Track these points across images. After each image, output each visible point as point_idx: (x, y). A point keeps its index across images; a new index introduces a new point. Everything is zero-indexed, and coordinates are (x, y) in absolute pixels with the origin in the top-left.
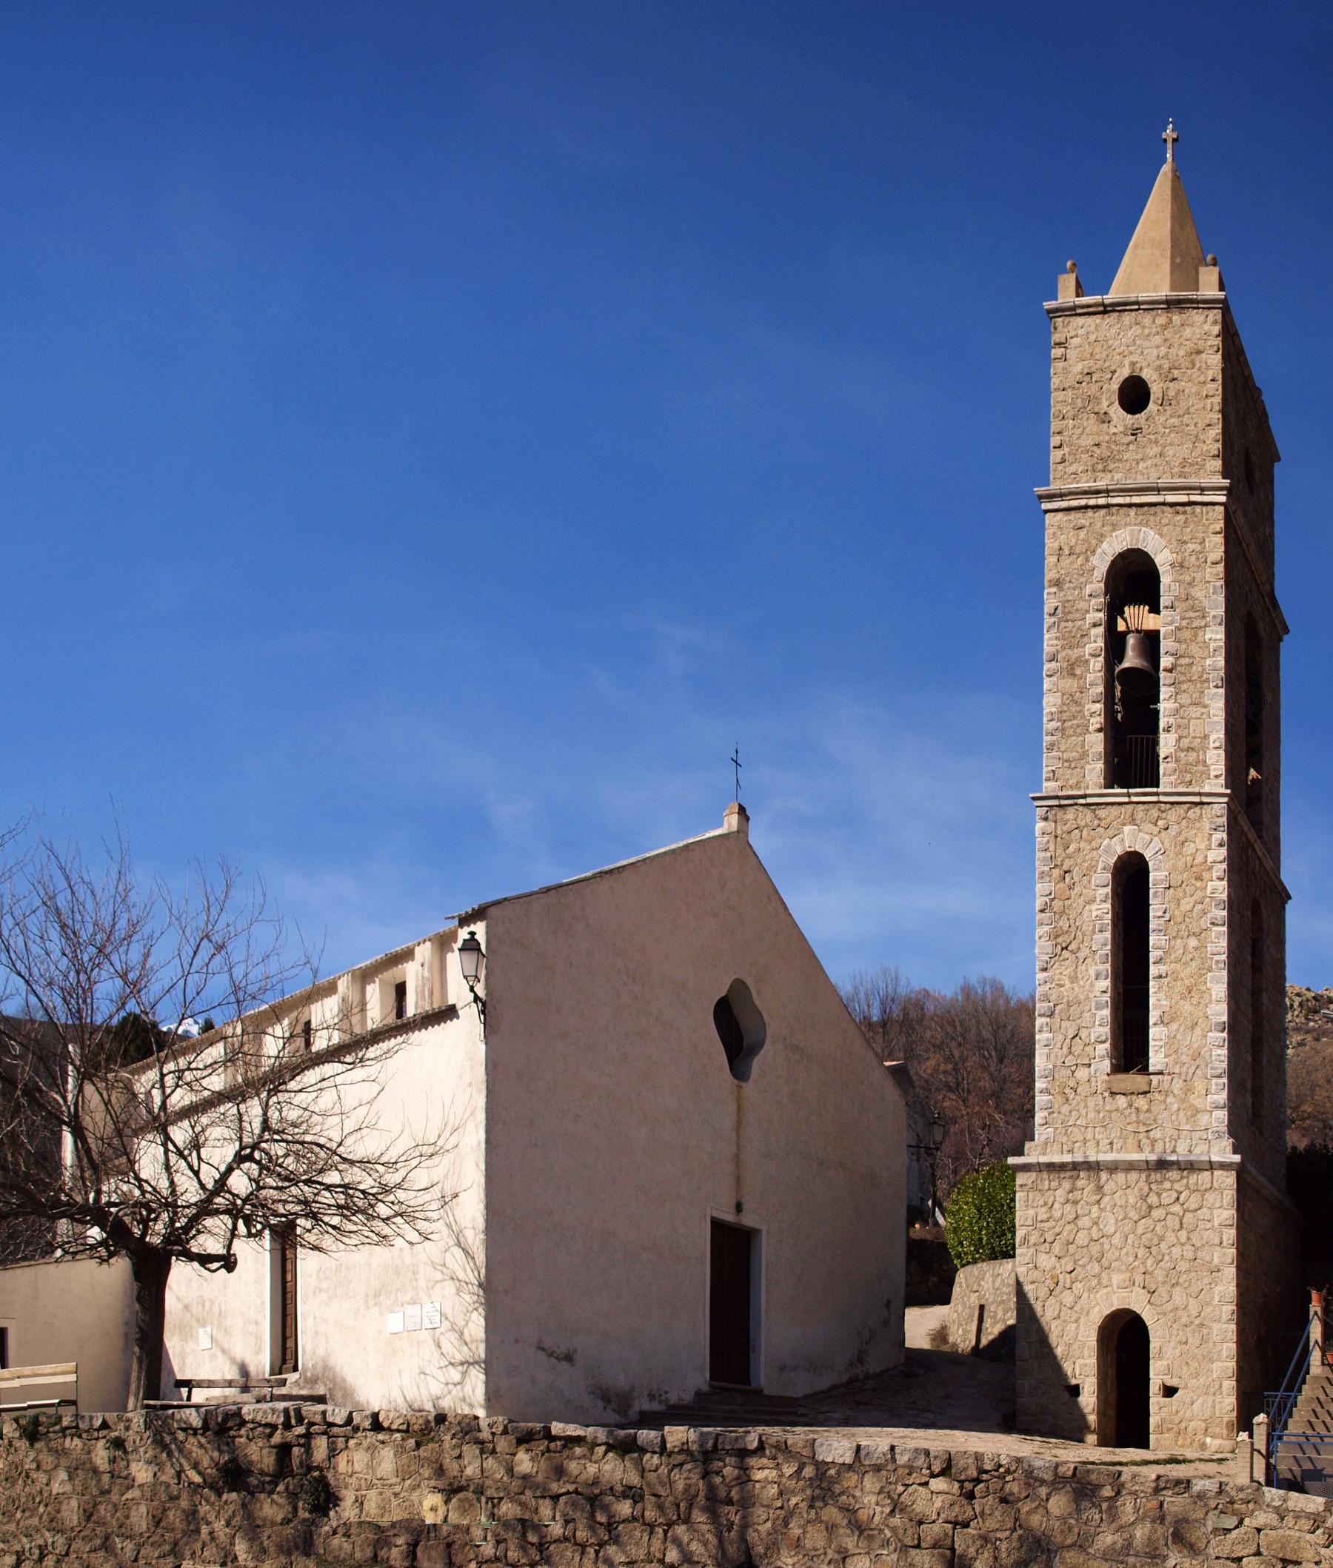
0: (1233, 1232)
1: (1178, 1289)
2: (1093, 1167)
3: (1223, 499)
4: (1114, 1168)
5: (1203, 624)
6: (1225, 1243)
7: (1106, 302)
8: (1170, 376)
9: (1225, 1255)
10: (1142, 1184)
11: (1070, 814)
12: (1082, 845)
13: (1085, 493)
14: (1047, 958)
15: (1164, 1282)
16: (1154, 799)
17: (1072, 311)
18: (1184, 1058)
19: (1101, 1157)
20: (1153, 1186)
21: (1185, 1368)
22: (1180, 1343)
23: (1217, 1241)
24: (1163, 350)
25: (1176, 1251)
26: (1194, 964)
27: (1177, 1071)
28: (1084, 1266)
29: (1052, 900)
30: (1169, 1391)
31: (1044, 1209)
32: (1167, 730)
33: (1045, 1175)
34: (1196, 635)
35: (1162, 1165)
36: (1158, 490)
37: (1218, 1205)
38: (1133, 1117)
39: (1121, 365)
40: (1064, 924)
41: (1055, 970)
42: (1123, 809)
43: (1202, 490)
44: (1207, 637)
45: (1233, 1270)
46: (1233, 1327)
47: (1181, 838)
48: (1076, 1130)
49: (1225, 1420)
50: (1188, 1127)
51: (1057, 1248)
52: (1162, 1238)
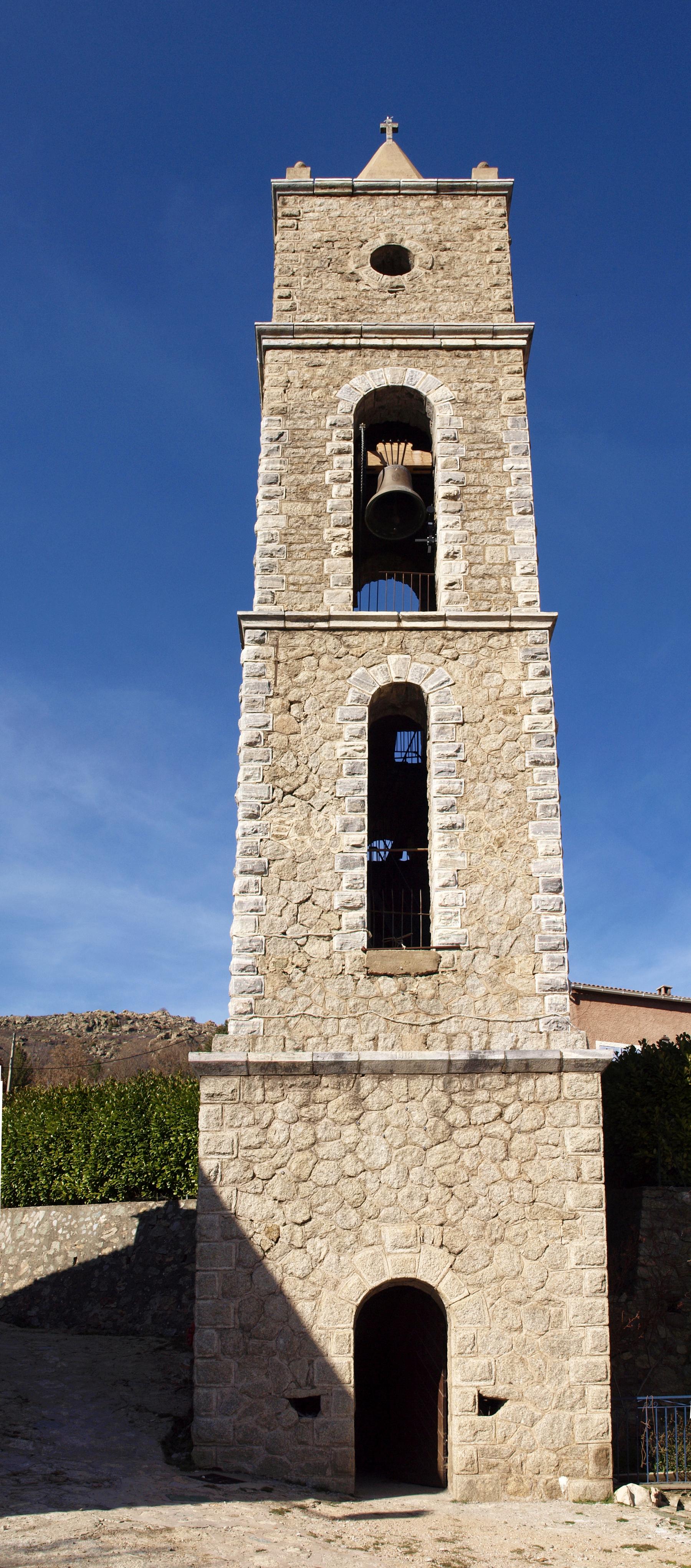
0: (599, 1160)
1: (502, 1246)
2: (347, 1071)
3: (524, 342)
4: (385, 1071)
5: (500, 454)
6: (585, 1177)
7: (356, 184)
8: (441, 247)
9: (586, 1193)
10: (435, 1094)
11: (301, 639)
12: (320, 673)
13: (329, 331)
14: (259, 802)
15: (479, 1238)
16: (439, 624)
17: (309, 191)
18: (494, 927)
19: (367, 1056)
20: (456, 1098)
21: (519, 1369)
22: (510, 1329)
23: (572, 1174)
24: (430, 227)
25: (499, 1191)
26: (506, 811)
27: (482, 943)
28: (328, 1215)
29: (270, 733)
30: (488, 1405)
31: (256, 1129)
32: (452, 556)
33: (256, 1081)
34: (489, 466)
35: (476, 1066)
36: (434, 333)
37: (570, 1122)
38: (409, 1005)
39: (375, 236)
40: (287, 762)
41: (272, 819)
42: (387, 636)
43: (495, 333)
44: (506, 467)
45: (600, 1217)
46: (603, 1302)
47: (480, 668)
48: (304, 1022)
49: (593, 1447)
50: (505, 1017)
51: (277, 1187)
52: (472, 1172)
